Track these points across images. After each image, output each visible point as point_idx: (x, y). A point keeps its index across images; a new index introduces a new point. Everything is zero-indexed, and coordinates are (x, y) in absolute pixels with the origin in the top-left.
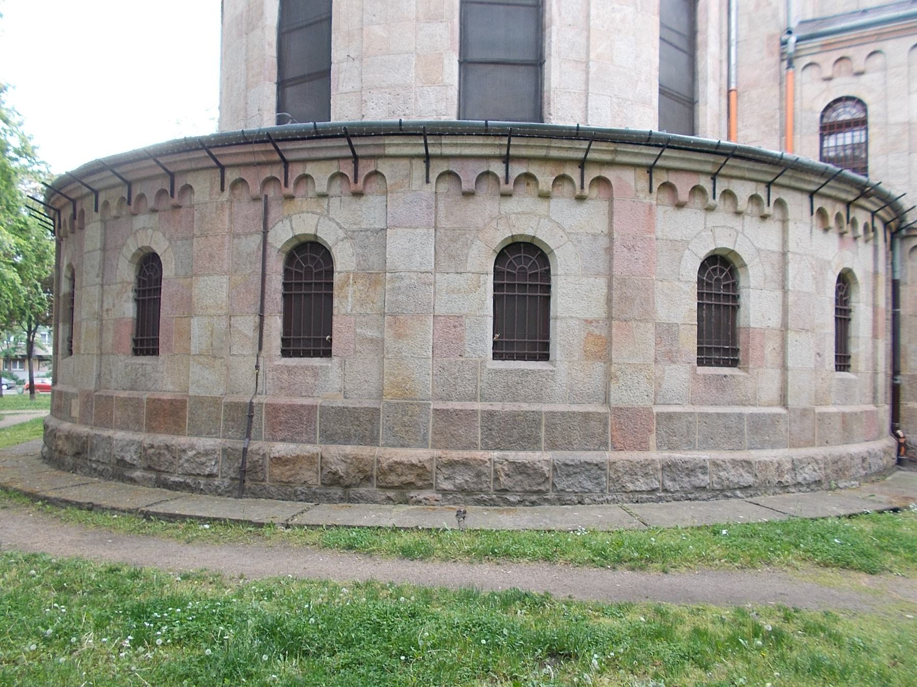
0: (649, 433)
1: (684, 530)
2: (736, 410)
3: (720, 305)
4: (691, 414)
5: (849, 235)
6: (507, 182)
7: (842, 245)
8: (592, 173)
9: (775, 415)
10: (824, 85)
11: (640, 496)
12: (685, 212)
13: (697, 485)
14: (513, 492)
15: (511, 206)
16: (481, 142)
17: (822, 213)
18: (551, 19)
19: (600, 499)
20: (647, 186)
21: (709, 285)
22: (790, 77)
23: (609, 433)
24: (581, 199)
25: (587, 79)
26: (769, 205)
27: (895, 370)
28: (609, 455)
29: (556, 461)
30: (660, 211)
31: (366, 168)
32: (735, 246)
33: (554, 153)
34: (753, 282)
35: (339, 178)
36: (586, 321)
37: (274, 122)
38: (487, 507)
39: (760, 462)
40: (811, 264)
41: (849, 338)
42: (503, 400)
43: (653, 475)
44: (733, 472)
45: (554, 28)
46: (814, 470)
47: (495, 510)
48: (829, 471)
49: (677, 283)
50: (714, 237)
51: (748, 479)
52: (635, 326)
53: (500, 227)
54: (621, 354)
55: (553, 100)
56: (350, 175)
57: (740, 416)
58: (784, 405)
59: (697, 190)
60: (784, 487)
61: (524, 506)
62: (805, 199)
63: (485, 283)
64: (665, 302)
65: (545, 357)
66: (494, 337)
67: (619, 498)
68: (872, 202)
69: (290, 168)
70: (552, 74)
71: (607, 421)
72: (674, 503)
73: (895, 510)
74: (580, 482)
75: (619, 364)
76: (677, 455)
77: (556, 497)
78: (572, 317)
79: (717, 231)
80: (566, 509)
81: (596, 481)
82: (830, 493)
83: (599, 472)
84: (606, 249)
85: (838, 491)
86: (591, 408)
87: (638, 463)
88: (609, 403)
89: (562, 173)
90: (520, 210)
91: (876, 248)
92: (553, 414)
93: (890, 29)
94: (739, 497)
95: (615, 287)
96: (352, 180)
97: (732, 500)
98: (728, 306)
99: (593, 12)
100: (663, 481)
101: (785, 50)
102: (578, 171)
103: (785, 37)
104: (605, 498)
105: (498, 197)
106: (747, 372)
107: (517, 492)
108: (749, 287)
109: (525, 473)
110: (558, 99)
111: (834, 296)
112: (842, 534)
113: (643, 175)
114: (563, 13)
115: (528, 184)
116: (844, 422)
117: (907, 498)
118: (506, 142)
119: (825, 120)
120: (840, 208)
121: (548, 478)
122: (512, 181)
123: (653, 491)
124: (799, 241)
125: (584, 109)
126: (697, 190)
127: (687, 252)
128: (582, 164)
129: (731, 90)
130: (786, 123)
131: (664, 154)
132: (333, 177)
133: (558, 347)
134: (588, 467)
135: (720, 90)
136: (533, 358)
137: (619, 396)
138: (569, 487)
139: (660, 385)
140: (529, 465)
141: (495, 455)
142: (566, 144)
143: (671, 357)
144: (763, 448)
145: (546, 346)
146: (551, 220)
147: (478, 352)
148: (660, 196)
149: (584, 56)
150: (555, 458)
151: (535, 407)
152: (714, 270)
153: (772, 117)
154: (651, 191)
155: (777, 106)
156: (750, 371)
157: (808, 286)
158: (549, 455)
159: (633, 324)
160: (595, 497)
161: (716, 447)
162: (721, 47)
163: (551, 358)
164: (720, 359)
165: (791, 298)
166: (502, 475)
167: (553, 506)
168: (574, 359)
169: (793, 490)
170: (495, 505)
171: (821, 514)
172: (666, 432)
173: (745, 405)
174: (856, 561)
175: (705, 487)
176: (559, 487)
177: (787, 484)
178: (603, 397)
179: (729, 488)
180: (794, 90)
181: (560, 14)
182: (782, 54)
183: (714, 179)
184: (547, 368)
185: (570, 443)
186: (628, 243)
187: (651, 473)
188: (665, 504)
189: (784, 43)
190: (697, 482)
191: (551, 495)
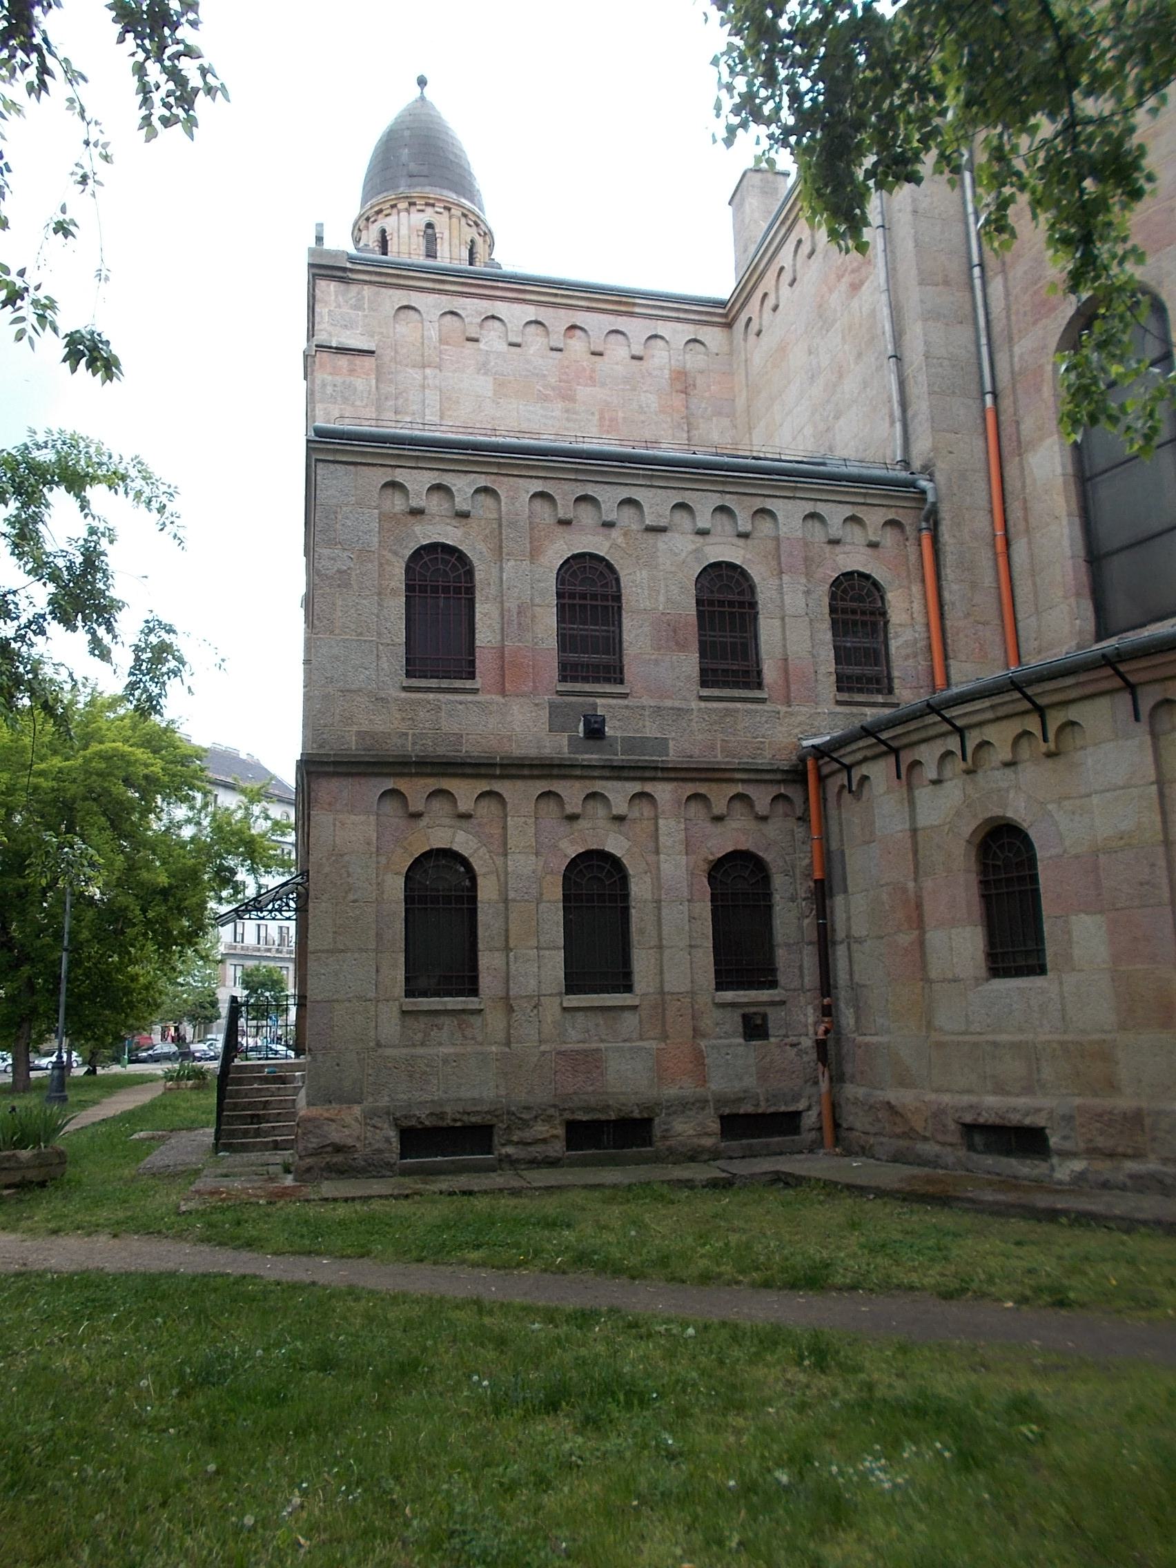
31: (1055, 719)
56: (1037, 731)
69: (967, 735)
132: (776, 798)
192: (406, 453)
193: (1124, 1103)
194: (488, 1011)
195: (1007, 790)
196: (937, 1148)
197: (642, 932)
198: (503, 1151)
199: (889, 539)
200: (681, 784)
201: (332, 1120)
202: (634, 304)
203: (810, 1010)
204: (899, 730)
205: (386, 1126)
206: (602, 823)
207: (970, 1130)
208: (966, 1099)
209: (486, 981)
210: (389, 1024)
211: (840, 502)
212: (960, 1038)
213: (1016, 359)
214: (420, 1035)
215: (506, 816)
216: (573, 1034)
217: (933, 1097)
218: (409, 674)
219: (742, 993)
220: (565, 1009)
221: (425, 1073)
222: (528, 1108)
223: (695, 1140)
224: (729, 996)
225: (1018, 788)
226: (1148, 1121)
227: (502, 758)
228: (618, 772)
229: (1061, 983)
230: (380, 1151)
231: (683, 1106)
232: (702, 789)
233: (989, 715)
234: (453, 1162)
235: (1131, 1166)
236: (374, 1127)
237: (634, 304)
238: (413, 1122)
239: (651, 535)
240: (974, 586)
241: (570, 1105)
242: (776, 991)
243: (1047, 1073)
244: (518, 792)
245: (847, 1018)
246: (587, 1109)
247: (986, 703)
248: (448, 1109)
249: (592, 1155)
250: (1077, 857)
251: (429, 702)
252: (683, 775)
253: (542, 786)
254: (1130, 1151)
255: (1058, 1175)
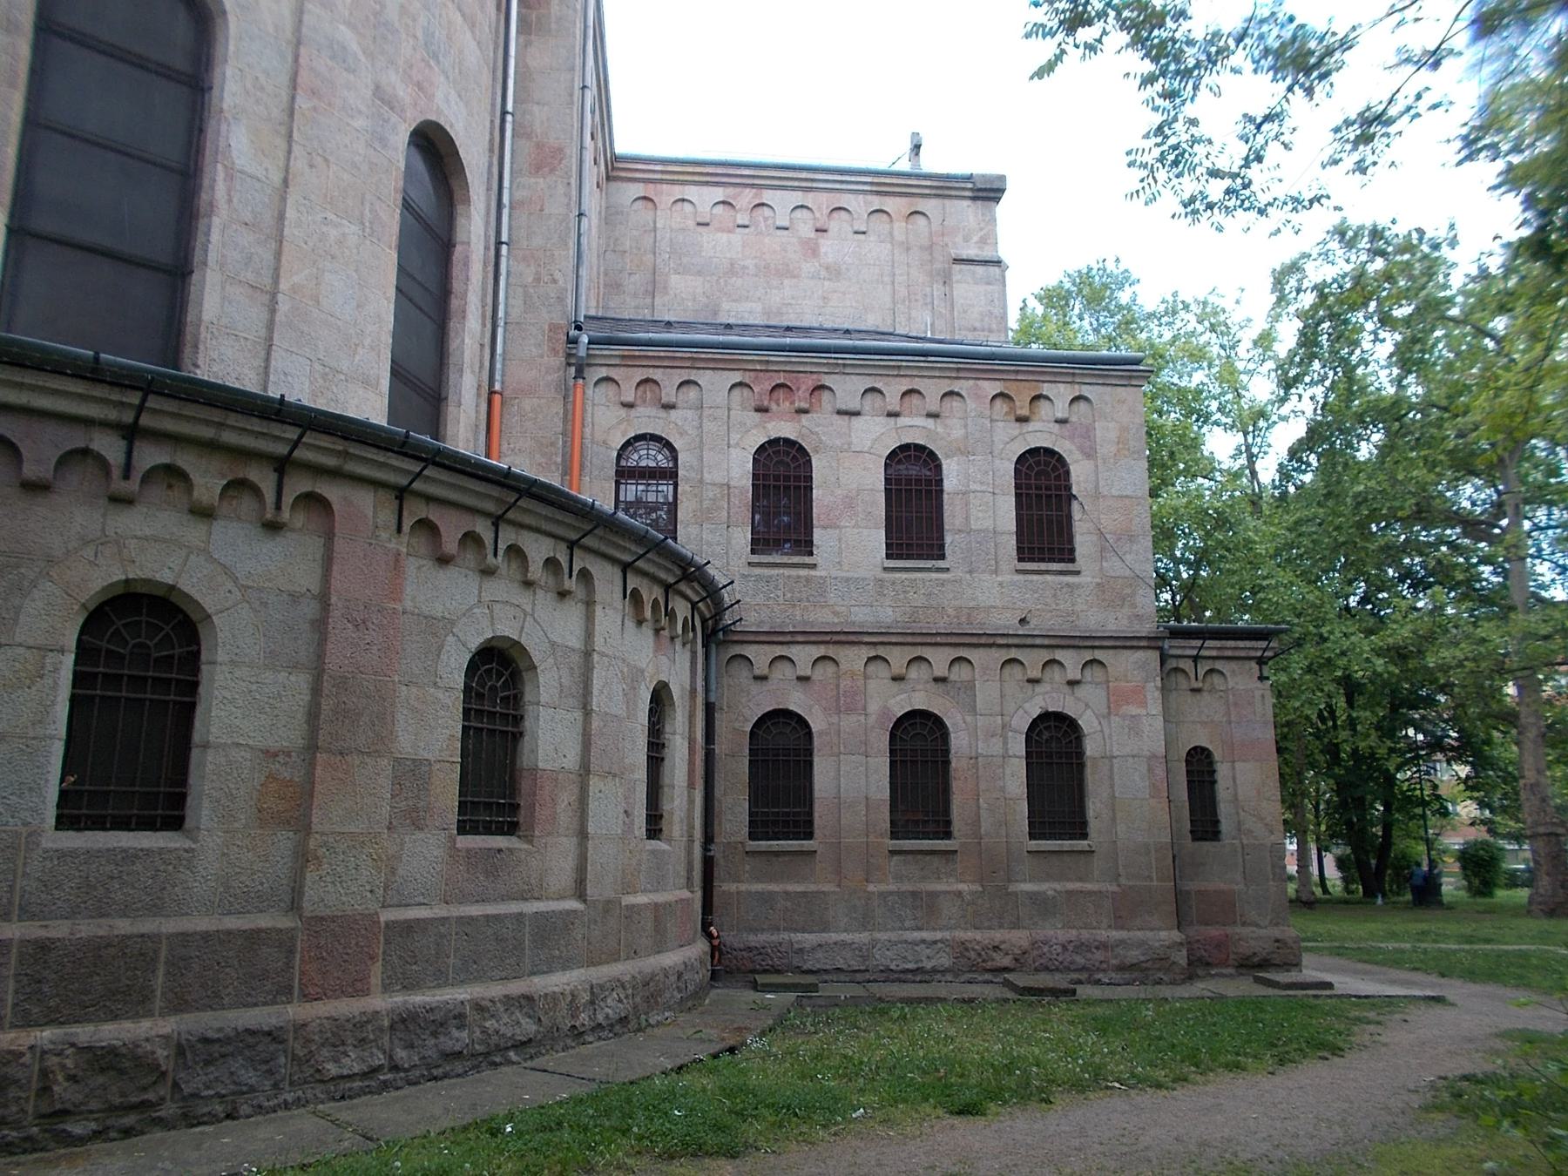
0: (369, 963)
1: (441, 1137)
2: (514, 907)
3: (495, 730)
4: (444, 920)
5: (666, 633)
6: (126, 475)
7: (658, 649)
8: (298, 485)
9: (569, 913)
10: (623, 412)
11: (348, 1085)
12: (452, 572)
13: (448, 1050)
14: (81, 1113)
15: (129, 522)
16: (80, 391)
17: (636, 598)
18: (211, 205)
19: (271, 1103)
20: (394, 522)
21: (480, 696)
22: (579, 390)
23: (297, 968)
24: (273, 527)
25: (270, 326)
26: (571, 576)
27: (708, 839)
28: (295, 1011)
29: (184, 1036)
30: (411, 566)
32: (520, 636)
33: (229, 437)
34: (544, 697)
36: (266, 752)
38: (15, 1159)
39: (546, 995)
40: (622, 672)
41: (662, 787)
42: (73, 914)
43: (375, 1040)
44: (505, 1019)
45: (216, 221)
46: (620, 1001)
47: (36, 1161)
48: (638, 999)
49: (432, 690)
50: (492, 617)
51: (529, 1027)
52: (357, 762)
53: (100, 561)
54: (328, 817)
55: (205, 343)
57: (520, 917)
58: (581, 895)
59: (470, 538)
60: (577, 1034)
61: (105, 1141)
62: (617, 573)
63: (56, 670)
64: (411, 721)
65: (175, 822)
66: (62, 780)
67: (309, 1095)
68: (693, 588)
70: (207, 297)
71: (294, 945)
72: (408, 1090)
73: (732, 1050)
74: (232, 1073)
75: (323, 834)
76: (418, 999)
77: (180, 1112)
78: (238, 745)
79: (497, 607)
80: (202, 1133)
81: (264, 1067)
82: (641, 1037)
83: (273, 1047)
84: (312, 622)
85: (649, 1030)
86: (264, 921)
87: (348, 1021)
88: (300, 908)
89: (241, 475)
90: (148, 532)
91: (694, 653)
92: (185, 937)
93: (710, 356)
94: (514, 1063)
95: (326, 692)
97: (504, 1069)
98: (507, 732)
99: (290, 214)
100: (391, 1050)
101: (574, 351)
102: (273, 477)
103: (573, 333)
104: (281, 1099)
105: (103, 502)
106: (531, 842)
107: (91, 1112)
108: (538, 703)
109: (113, 1068)
110: (214, 342)
111: (646, 723)
112: (682, 1099)
113: (388, 498)
114: (235, 200)
115: (170, 486)
116: (656, 919)
117: (739, 1029)
118: (136, 401)
119: (623, 463)
120: (658, 592)
121: (164, 1074)
122: (137, 476)
123: (375, 1070)
124: (607, 635)
125: (261, 370)
126: (470, 538)
127: (450, 638)
128: (282, 465)
129: (495, 392)
130: (572, 456)
131: (426, 472)
133: (206, 803)
134: (251, 1040)
135: (479, 386)
136: (148, 824)
137: (321, 894)
138: (208, 1088)
139: (393, 871)
140: (124, 1051)
141: (46, 1035)
142: (256, 425)
143: (415, 819)
144: (550, 971)
145: (179, 800)
146: (211, 559)
147: (23, 814)
148: (414, 541)
149: (267, 281)
150: (183, 1027)
151: (148, 926)
152: (489, 671)
153: (552, 444)
154: (399, 530)
155: (560, 429)
156: (535, 840)
157: (619, 709)
158: (169, 1025)
159: (356, 760)
160: (262, 1100)
161: (480, 977)
162: (484, 325)
163: (188, 823)
164: (491, 822)
165: (596, 723)
166: (60, 1078)
167: (173, 1133)
168: (236, 825)
169: (590, 1039)
170: (35, 1150)
171: (638, 1073)
172: (400, 957)
173: (526, 899)
174: (711, 1140)
175: (461, 1052)
176: (187, 1089)
177: (583, 1029)
178: (288, 898)
179: (498, 1049)
180: (584, 410)
181: (230, 201)
182: (569, 355)
183: (496, 525)
184: (178, 845)
185: (217, 995)
186: (355, 614)
187: (372, 1037)
188: (394, 1094)
189: (573, 341)
190: (448, 1044)
191: (169, 1110)
192: (745, 357)
218: (1020, 560)
232: (831, 651)
242: (1086, 842)
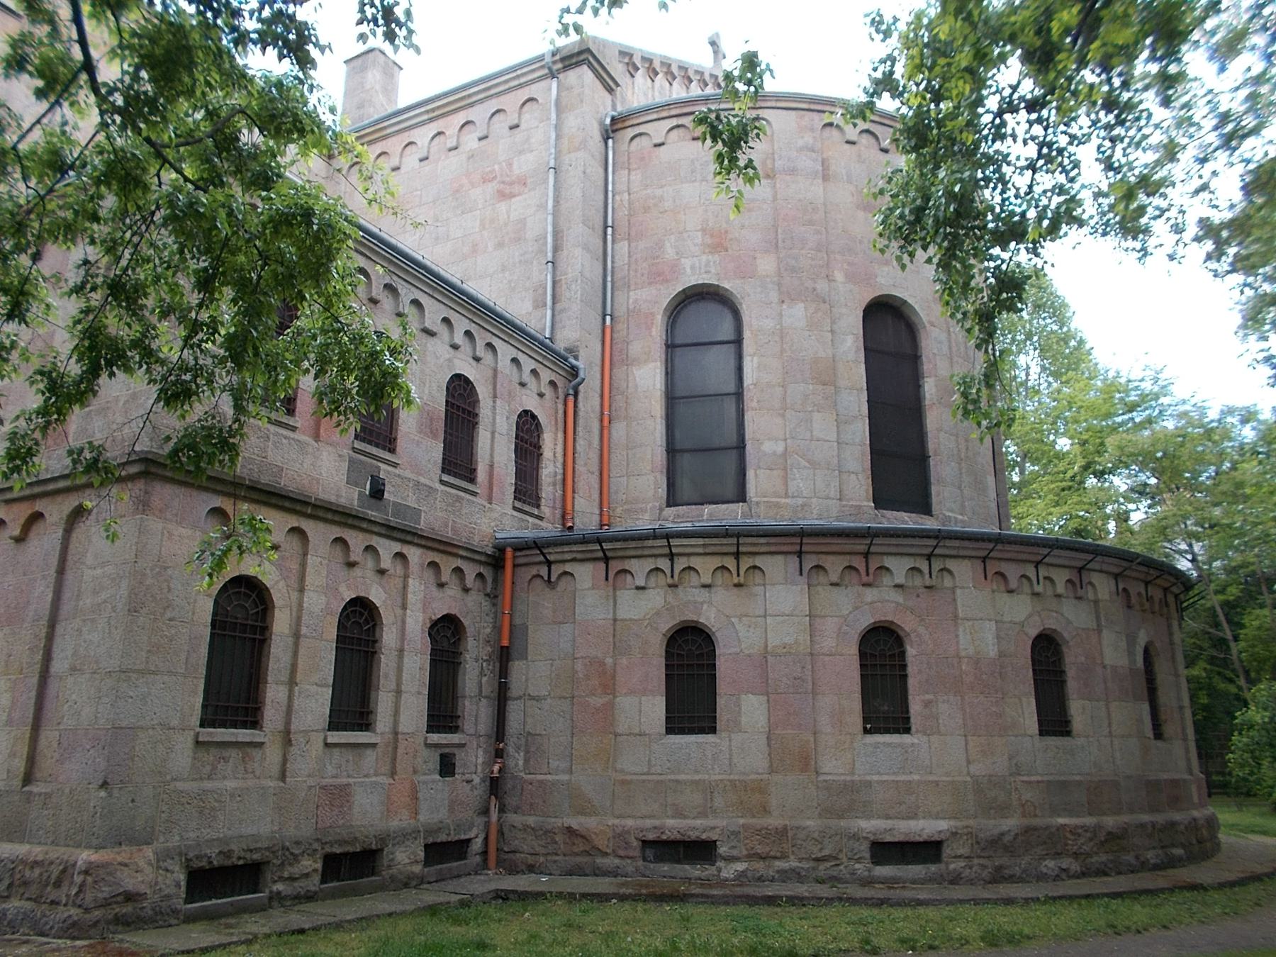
35: (751, 571)
37: (860, 487)
96: (669, 574)
193: (774, 821)
194: (268, 745)
195: (702, 604)
196: (617, 861)
197: (386, 676)
198: (275, 888)
199: (547, 391)
200: (425, 551)
201: (126, 865)
202: (385, 128)
203: (480, 752)
204: (618, 545)
205: (177, 868)
206: (370, 574)
207: (645, 843)
208: (649, 823)
209: (272, 715)
210: (182, 755)
211: (530, 357)
212: (644, 777)
213: (631, 301)
214: (208, 768)
215: (305, 554)
216: (330, 770)
217: (616, 821)
219: (444, 735)
220: (327, 745)
221: (213, 809)
222: (298, 843)
223: (409, 868)
224: (435, 738)
225: (710, 603)
226: (790, 834)
227: (316, 499)
228: (391, 531)
229: (730, 740)
230: (168, 897)
231: (404, 836)
233: (701, 550)
234: (232, 904)
235: (779, 864)
236: (167, 870)
237: (385, 128)
238: (204, 863)
239: (424, 335)
240: (590, 444)
241: (330, 838)
243: (719, 802)
244: (321, 535)
245: (516, 760)
246: (342, 842)
247: (701, 541)
248: (233, 847)
249: (334, 887)
250: (749, 656)
251: (259, 429)
252: (430, 544)
253: (337, 532)
254: (779, 854)
255: (724, 874)
